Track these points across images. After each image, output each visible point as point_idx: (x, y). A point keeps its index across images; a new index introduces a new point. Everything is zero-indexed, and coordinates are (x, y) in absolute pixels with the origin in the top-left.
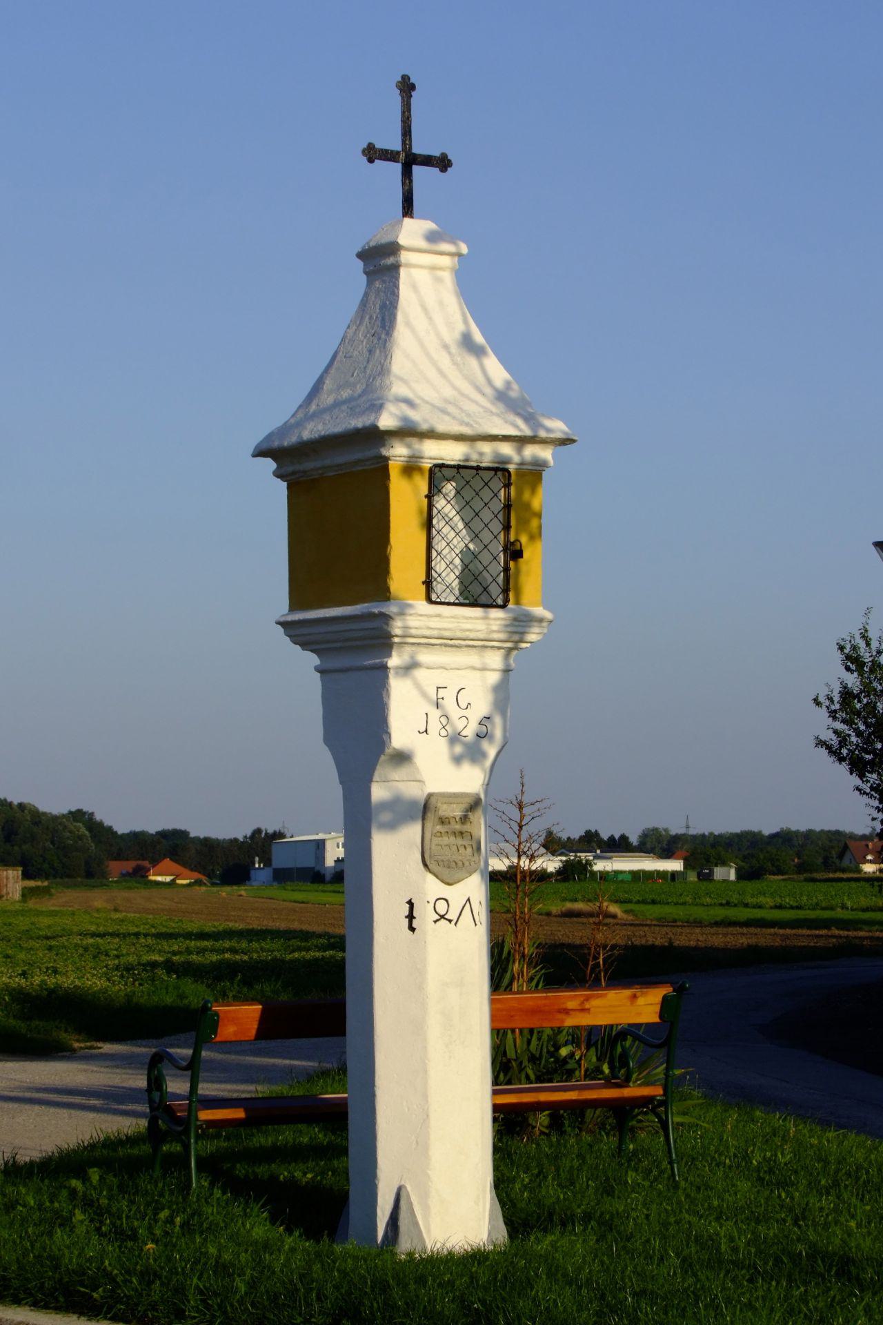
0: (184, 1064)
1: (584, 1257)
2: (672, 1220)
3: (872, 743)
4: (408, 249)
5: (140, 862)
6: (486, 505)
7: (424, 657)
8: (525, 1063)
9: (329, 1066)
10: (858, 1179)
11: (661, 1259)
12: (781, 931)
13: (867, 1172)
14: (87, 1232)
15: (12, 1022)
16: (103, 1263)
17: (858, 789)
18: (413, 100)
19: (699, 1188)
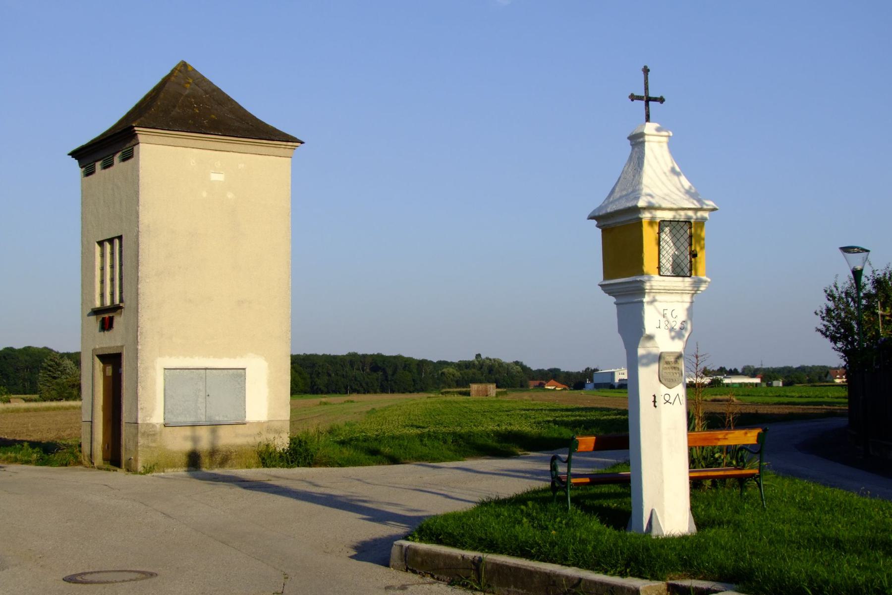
0: (565, 460)
1: (728, 538)
2: (764, 523)
3: (839, 330)
4: (648, 135)
5: (542, 381)
6: (682, 236)
7: (658, 297)
8: (701, 460)
9: (620, 461)
10: (841, 507)
11: (760, 540)
12: (802, 407)
13: (845, 505)
14: (528, 526)
16: (535, 538)
17: (833, 348)
18: (649, 76)
19: (774, 511)
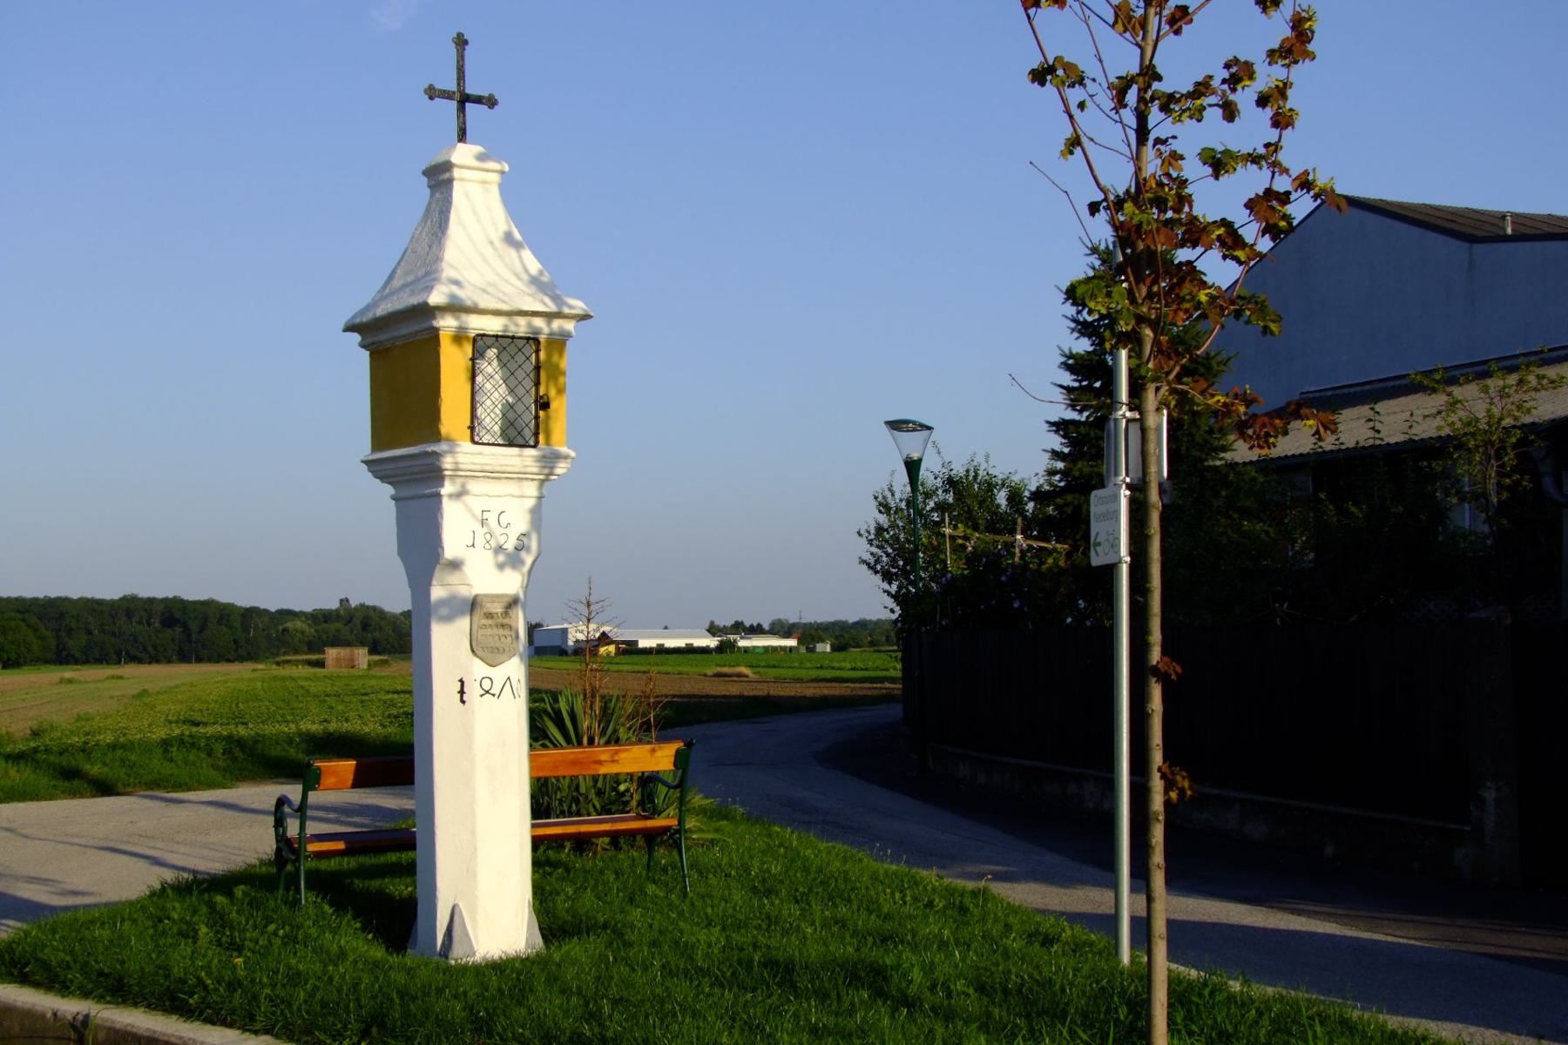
7: (473, 486)
12: (852, 685)
13: (836, 881)
15: (301, 756)
